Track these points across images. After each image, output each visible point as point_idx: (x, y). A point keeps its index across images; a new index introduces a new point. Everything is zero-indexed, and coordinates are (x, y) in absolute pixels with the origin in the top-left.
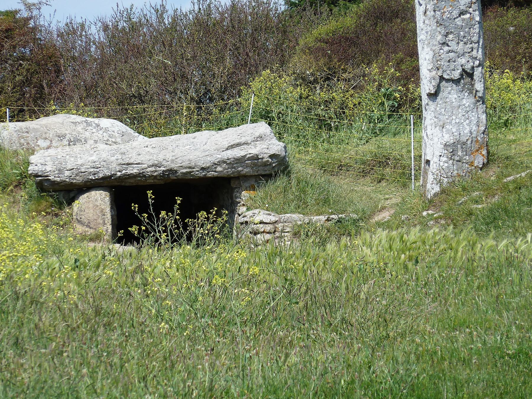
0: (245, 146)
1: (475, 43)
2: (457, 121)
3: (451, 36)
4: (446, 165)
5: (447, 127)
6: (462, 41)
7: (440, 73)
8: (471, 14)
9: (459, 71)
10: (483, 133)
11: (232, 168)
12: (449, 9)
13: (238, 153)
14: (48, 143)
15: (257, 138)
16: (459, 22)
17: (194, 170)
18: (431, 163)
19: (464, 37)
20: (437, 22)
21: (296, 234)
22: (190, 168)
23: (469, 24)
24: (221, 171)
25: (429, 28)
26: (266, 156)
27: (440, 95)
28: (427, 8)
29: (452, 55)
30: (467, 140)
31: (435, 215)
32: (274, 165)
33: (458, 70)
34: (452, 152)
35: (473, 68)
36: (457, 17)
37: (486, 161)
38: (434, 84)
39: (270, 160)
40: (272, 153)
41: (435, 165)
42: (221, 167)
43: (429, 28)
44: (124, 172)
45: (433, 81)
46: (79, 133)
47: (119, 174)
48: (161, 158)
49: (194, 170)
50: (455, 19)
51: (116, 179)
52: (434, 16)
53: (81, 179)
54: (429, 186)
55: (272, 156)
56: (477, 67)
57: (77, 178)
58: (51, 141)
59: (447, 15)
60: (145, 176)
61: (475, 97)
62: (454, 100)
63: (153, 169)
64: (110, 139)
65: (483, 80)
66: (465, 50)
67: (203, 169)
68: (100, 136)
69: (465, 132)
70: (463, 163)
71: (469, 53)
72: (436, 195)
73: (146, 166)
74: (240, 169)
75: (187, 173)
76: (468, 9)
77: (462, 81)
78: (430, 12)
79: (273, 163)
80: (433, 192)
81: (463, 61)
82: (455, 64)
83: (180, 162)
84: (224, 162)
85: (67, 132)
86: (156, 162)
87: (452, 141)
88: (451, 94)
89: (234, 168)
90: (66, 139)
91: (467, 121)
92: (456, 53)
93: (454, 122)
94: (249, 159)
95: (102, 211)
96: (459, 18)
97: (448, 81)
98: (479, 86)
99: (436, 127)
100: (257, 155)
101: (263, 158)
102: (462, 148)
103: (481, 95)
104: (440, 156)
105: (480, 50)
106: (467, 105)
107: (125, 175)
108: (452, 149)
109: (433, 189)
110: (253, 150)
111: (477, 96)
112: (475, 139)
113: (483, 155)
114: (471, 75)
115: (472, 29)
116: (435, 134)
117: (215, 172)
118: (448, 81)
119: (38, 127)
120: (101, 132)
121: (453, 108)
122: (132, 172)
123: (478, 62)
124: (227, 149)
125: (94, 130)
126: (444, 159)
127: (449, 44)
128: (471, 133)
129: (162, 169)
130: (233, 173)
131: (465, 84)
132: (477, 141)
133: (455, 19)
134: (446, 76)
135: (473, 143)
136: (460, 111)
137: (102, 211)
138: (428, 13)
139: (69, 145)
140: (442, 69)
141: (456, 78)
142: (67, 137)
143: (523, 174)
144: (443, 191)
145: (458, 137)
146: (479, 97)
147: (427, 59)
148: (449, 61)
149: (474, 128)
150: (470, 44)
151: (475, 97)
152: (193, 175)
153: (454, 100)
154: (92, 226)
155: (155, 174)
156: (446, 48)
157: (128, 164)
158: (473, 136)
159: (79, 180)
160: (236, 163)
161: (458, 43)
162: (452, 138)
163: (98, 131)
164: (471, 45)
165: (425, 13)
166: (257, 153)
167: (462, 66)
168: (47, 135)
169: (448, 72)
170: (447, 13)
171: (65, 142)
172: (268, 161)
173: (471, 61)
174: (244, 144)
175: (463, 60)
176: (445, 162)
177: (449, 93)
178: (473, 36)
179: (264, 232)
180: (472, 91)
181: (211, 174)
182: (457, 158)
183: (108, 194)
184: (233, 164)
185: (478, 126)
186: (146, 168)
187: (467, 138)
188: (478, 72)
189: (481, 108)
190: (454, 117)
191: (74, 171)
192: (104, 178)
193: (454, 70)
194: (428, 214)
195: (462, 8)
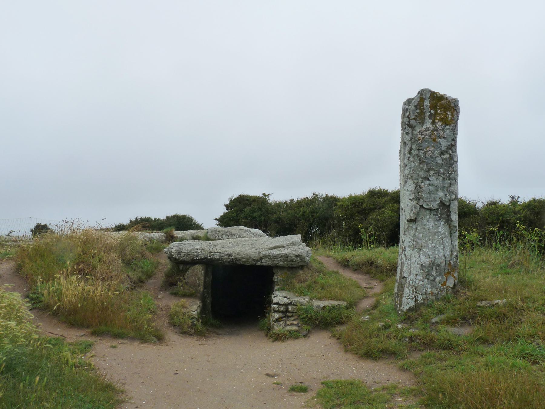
2: (434, 245)
3: (432, 172)
4: (421, 283)
5: (424, 250)
9: (437, 203)
13: (276, 252)
19: (444, 174)
25: (413, 164)
29: (431, 188)
40: (297, 254)
48: (232, 250)
54: (404, 300)
62: (431, 227)
67: (254, 260)
71: (447, 187)
72: (410, 310)
75: (245, 262)
80: (408, 306)
81: (441, 194)
88: (430, 222)
94: (282, 256)
99: (414, 249)
104: (417, 274)
106: (442, 233)
108: (428, 270)
110: (285, 251)
112: (448, 263)
113: (455, 277)
126: (420, 277)
127: (430, 179)
131: (441, 214)
134: (425, 206)
138: (413, 151)
145: (433, 259)
153: (431, 227)
155: (229, 260)
157: (215, 253)
159: (188, 259)
177: (428, 221)
178: (451, 174)
190: (431, 242)
192: (202, 259)
195: (443, 149)
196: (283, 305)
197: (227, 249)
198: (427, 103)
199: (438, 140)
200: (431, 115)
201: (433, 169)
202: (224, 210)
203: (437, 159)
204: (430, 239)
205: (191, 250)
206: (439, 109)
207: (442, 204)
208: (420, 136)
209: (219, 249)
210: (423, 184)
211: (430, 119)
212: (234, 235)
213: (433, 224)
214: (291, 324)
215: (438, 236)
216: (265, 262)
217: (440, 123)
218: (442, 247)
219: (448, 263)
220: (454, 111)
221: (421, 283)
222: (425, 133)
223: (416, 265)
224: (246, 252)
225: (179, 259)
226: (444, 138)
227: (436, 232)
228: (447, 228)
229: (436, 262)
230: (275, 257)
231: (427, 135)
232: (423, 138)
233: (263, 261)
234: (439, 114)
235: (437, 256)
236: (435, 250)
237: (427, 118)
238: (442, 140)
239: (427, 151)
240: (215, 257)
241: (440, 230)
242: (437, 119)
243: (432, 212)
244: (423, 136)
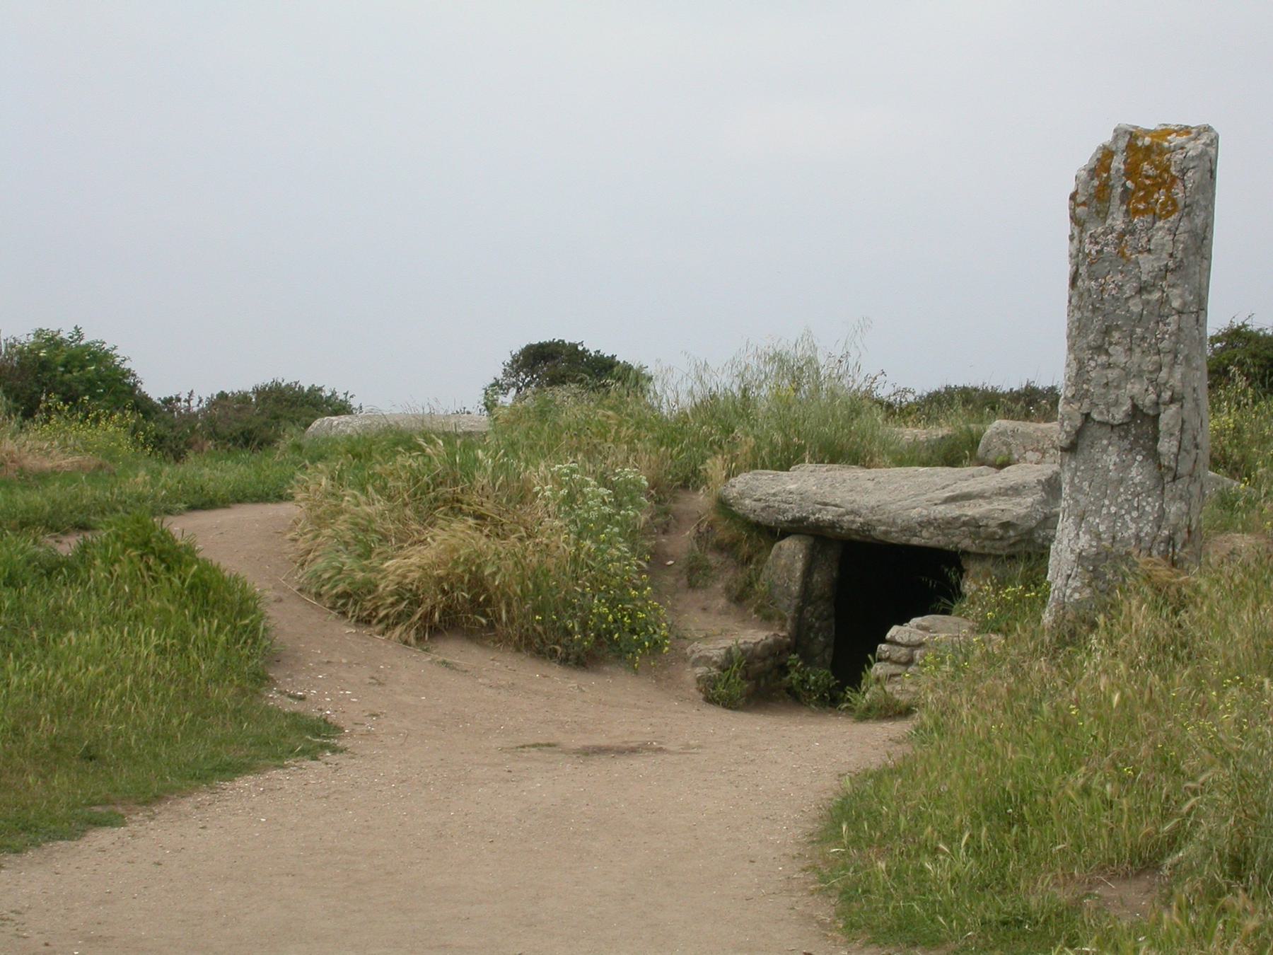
2: (1113, 509)
5: (1091, 519)
13: (953, 511)
19: (1143, 339)
21: (980, 676)
29: (1112, 374)
38: (1068, 429)
39: (1000, 532)
47: (812, 518)
55: (1006, 525)
62: (1111, 467)
63: (851, 518)
75: (886, 533)
81: (1134, 388)
84: (930, 523)
93: (1104, 511)
94: (964, 524)
101: (987, 526)
104: (1069, 576)
107: (817, 520)
110: (971, 510)
129: (861, 520)
131: (1137, 438)
133: (1127, 299)
138: (1079, 283)
157: (826, 504)
159: (763, 517)
162: (1094, 543)
167: (1132, 398)
172: (995, 533)
175: (1137, 386)
176: (1075, 590)
178: (1163, 339)
179: (888, 659)
181: (915, 541)
190: (1107, 502)
192: (794, 521)
195: (1144, 278)
198: (1118, 163)
200: (1126, 195)
201: (1118, 327)
203: (1131, 303)
204: (1106, 496)
205: (774, 495)
207: (1136, 411)
210: (1093, 364)
211: (1122, 202)
212: (268, 495)
213: (1115, 458)
215: (1127, 489)
216: (925, 538)
218: (1135, 514)
221: (1077, 596)
222: (1101, 240)
226: (1149, 251)
228: (1150, 467)
230: (950, 523)
231: (1107, 245)
233: (925, 534)
236: (1115, 522)
238: (1142, 258)
240: (827, 516)
241: (1134, 473)
243: (1116, 430)
244: (1098, 248)
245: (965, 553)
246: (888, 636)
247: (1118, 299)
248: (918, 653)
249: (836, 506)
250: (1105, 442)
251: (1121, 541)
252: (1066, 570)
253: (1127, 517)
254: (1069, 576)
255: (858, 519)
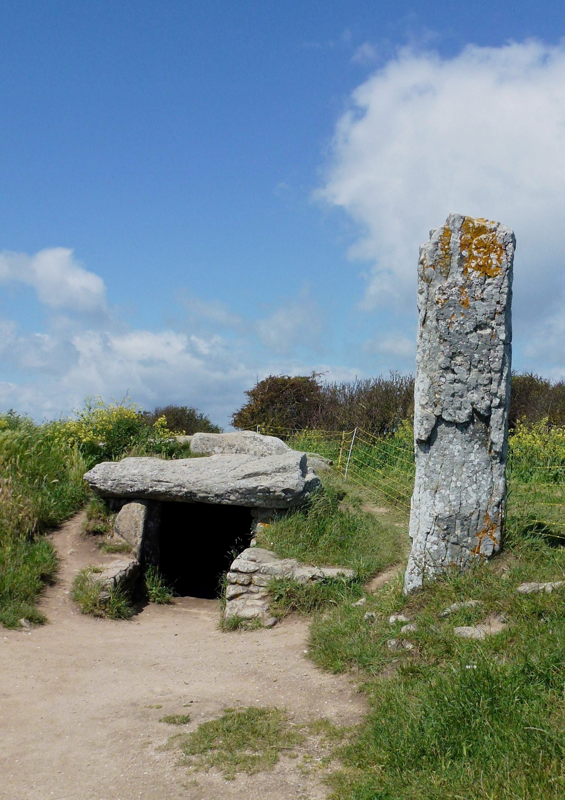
0: (265, 477)
1: (496, 372)
2: (459, 484)
3: (459, 359)
4: (435, 547)
5: (443, 491)
6: (476, 367)
7: (437, 412)
8: (493, 328)
9: (467, 411)
10: (498, 506)
11: (245, 498)
12: (459, 319)
13: (251, 483)
14: (221, 450)
15: (280, 469)
16: (473, 339)
17: (209, 495)
18: (415, 541)
19: (480, 361)
20: (440, 337)
22: (206, 493)
23: (488, 343)
24: (234, 500)
25: (428, 345)
26: (278, 489)
27: (436, 443)
28: (428, 315)
29: (458, 386)
30: (472, 514)
31: (404, 629)
32: (288, 500)
33: (466, 409)
34: (445, 530)
35: (489, 409)
36: (471, 332)
37: (497, 547)
38: (427, 427)
39: (283, 494)
40: (285, 487)
41: (418, 544)
42: (234, 496)
43: (428, 345)
44: (154, 488)
45: (425, 422)
46: (246, 445)
47: (151, 489)
49: (209, 495)
50: (467, 334)
51: (148, 494)
52: (436, 328)
53: (121, 490)
55: (285, 491)
56: (495, 408)
57: (117, 488)
58: (224, 449)
59: (455, 327)
60: (171, 495)
61: (490, 451)
63: (178, 489)
64: (268, 452)
65: (503, 428)
66: (479, 381)
68: (261, 448)
69: (469, 502)
70: (462, 547)
71: (485, 385)
73: (172, 485)
74: (253, 500)
76: (489, 321)
77: (471, 426)
78: (431, 321)
79: (288, 498)
80: (410, 586)
82: (462, 400)
83: (200, 485)
85: (236, 443)
86: (181, 483)
87: (448, 513)
88: (452, 443)
89: (247, 498)
90: (235, 448)
91: (474, 486)
92: (465, 384)
93: (453, 485)
94: (260, 491)
95: (136, 523)
96: (474, 334)
97: (449, 424)
98: (497, 436)
99: (425, 490)
100: (269, 489)
101: (275, 492)
102: (462, 524)
103: (498, 450)
104: (428, 533)
105: (503, 384)
106: (475, 463)
107: (155, 491)
108: (446, 525)
109: (412, 581)
110: (264, 483)
111: (492, 451)
112: (483, 514)
113: (494, 539)
114: (486, 420)
115: (492, 351)
116: (423, 501)
117: (229, 500)
118: (449, 424)
119: (216, 437)
120: (262, 446)
121: (453, 464)
122: (160, 489)
123: (498, 400)
124: (244, 478)
125: (258, 444)
126: (434, 538)
128: (478, 504)
129: (185, 490)
130: (246, 503)
131: (475, 432)
132: (487, 517)
133: (467, 334)
134: (445, 417)
135: (481, 519)
136: (464, 469)
137: (136, 523)
138: (428, 322)
139: (236, 453)
140: (442, 405)
141: (461, 421)
142: (236, 448)
143: (548, 587)
144: (424, 588)
145: (457, 508)
146: (495, 452)
147: (421, 389)
148: (453, 395)
149: (484, 497)
150: (488, 373)
151: (490, 451)
152: (209, 501)
154: (125, 536)
155: (180, 494)
156: (450, 376)
157: (159, 481)
158: (481, 508)
159: (118, 490)
160: (249, 494)
161: (470, 370)
163: (260, 445)
164: (489, 374)
165: (424, 322)
166: (269, 486)
167: (472, 404)
168: (222, 444)
169: (450, 411)
170: (456, 324)
171: (234, 451)
172: (280, 495)
173: (486, 397)
174: (263, 474)
176: (434, 543)
177: (450, 442)
178: (494, 361)
179: (235, 583)
180: (486, 442)
181: (225, 502)
182: (453, 539)
183: (144, 507)
184: (245, 495)
185: (491, 495)
186: (173, 488)
187: (472, 511)
188: (497, 416)
189: (498, 469)
190: (454, 479)
191: (115, 482)
192: (139, 492)
193: (460, 409)
194: (397, 621)
195: (480, 318)
196: (246, 573)
197: (178, 476)
199: (471, 304)
202: (244, 401)
206: (477, 248)
208: (440, 296)
209: (168, 476)
211: (460, 265)
214: (252, 606)
217: (476, 274)
219: (483, 514)
220: (501, 252)
221: (435, 547)
222: (448, 291)
223: (427, 517)
224: (205, 482)
225: (106, 491)
227: (464, 463)
229: (461, 513)
231: (452, 295)
232: (445, 300)
234: (476, 258)
235: (464, 503)
237: (455, 264)
239: (452, 323)
242: (471, 267)
244: (445, 297)
245: (256, 508)
246: (233, 567)
247: (460, 334)
248: (255, 577)
249: (167, 482)
250: (451, 436)
251: (466, 506)
252: (424, 529)
253: (469, 489)
254: (428, 533)
255: (182, 489)
